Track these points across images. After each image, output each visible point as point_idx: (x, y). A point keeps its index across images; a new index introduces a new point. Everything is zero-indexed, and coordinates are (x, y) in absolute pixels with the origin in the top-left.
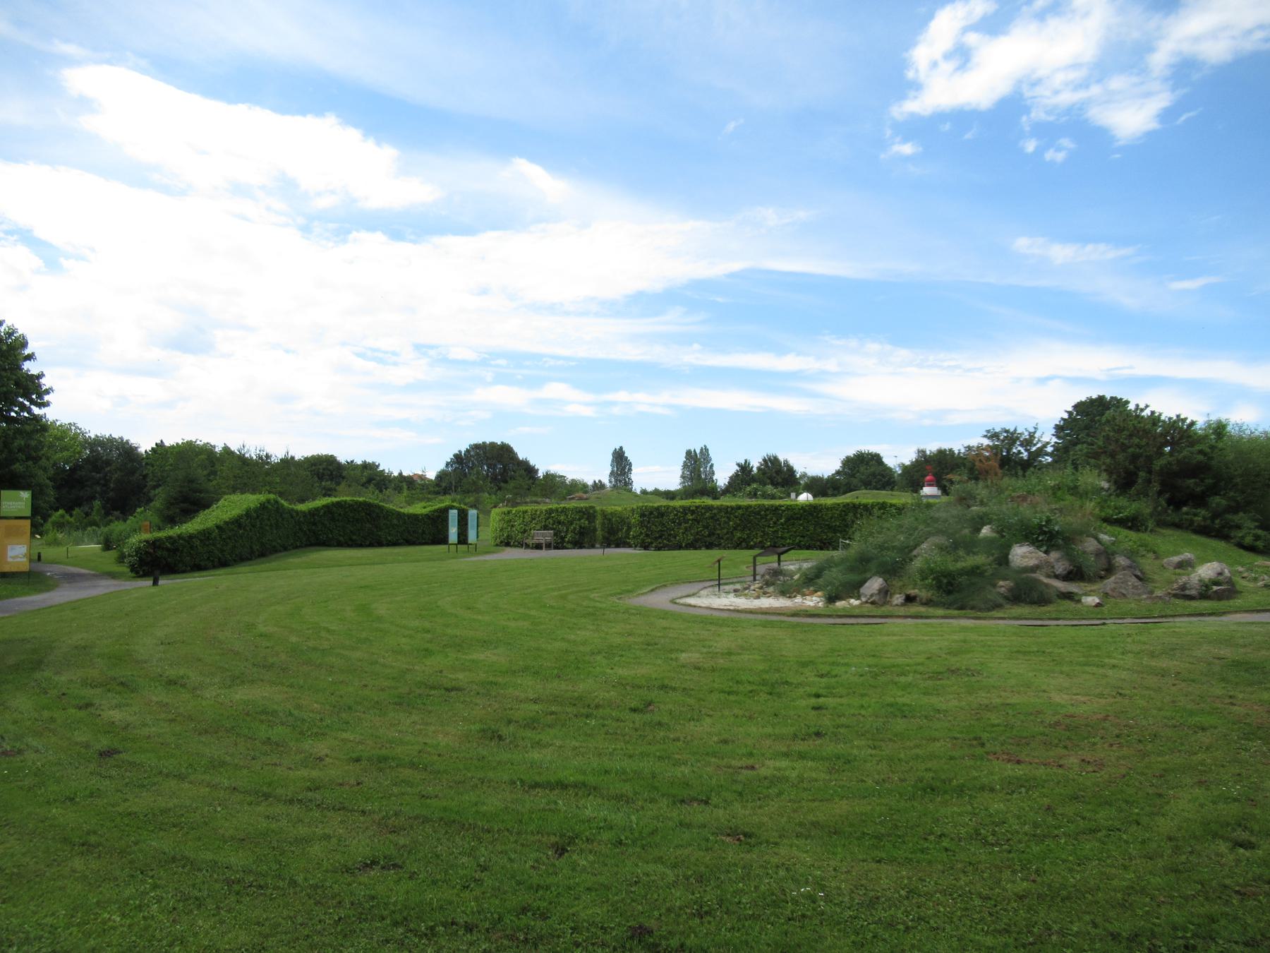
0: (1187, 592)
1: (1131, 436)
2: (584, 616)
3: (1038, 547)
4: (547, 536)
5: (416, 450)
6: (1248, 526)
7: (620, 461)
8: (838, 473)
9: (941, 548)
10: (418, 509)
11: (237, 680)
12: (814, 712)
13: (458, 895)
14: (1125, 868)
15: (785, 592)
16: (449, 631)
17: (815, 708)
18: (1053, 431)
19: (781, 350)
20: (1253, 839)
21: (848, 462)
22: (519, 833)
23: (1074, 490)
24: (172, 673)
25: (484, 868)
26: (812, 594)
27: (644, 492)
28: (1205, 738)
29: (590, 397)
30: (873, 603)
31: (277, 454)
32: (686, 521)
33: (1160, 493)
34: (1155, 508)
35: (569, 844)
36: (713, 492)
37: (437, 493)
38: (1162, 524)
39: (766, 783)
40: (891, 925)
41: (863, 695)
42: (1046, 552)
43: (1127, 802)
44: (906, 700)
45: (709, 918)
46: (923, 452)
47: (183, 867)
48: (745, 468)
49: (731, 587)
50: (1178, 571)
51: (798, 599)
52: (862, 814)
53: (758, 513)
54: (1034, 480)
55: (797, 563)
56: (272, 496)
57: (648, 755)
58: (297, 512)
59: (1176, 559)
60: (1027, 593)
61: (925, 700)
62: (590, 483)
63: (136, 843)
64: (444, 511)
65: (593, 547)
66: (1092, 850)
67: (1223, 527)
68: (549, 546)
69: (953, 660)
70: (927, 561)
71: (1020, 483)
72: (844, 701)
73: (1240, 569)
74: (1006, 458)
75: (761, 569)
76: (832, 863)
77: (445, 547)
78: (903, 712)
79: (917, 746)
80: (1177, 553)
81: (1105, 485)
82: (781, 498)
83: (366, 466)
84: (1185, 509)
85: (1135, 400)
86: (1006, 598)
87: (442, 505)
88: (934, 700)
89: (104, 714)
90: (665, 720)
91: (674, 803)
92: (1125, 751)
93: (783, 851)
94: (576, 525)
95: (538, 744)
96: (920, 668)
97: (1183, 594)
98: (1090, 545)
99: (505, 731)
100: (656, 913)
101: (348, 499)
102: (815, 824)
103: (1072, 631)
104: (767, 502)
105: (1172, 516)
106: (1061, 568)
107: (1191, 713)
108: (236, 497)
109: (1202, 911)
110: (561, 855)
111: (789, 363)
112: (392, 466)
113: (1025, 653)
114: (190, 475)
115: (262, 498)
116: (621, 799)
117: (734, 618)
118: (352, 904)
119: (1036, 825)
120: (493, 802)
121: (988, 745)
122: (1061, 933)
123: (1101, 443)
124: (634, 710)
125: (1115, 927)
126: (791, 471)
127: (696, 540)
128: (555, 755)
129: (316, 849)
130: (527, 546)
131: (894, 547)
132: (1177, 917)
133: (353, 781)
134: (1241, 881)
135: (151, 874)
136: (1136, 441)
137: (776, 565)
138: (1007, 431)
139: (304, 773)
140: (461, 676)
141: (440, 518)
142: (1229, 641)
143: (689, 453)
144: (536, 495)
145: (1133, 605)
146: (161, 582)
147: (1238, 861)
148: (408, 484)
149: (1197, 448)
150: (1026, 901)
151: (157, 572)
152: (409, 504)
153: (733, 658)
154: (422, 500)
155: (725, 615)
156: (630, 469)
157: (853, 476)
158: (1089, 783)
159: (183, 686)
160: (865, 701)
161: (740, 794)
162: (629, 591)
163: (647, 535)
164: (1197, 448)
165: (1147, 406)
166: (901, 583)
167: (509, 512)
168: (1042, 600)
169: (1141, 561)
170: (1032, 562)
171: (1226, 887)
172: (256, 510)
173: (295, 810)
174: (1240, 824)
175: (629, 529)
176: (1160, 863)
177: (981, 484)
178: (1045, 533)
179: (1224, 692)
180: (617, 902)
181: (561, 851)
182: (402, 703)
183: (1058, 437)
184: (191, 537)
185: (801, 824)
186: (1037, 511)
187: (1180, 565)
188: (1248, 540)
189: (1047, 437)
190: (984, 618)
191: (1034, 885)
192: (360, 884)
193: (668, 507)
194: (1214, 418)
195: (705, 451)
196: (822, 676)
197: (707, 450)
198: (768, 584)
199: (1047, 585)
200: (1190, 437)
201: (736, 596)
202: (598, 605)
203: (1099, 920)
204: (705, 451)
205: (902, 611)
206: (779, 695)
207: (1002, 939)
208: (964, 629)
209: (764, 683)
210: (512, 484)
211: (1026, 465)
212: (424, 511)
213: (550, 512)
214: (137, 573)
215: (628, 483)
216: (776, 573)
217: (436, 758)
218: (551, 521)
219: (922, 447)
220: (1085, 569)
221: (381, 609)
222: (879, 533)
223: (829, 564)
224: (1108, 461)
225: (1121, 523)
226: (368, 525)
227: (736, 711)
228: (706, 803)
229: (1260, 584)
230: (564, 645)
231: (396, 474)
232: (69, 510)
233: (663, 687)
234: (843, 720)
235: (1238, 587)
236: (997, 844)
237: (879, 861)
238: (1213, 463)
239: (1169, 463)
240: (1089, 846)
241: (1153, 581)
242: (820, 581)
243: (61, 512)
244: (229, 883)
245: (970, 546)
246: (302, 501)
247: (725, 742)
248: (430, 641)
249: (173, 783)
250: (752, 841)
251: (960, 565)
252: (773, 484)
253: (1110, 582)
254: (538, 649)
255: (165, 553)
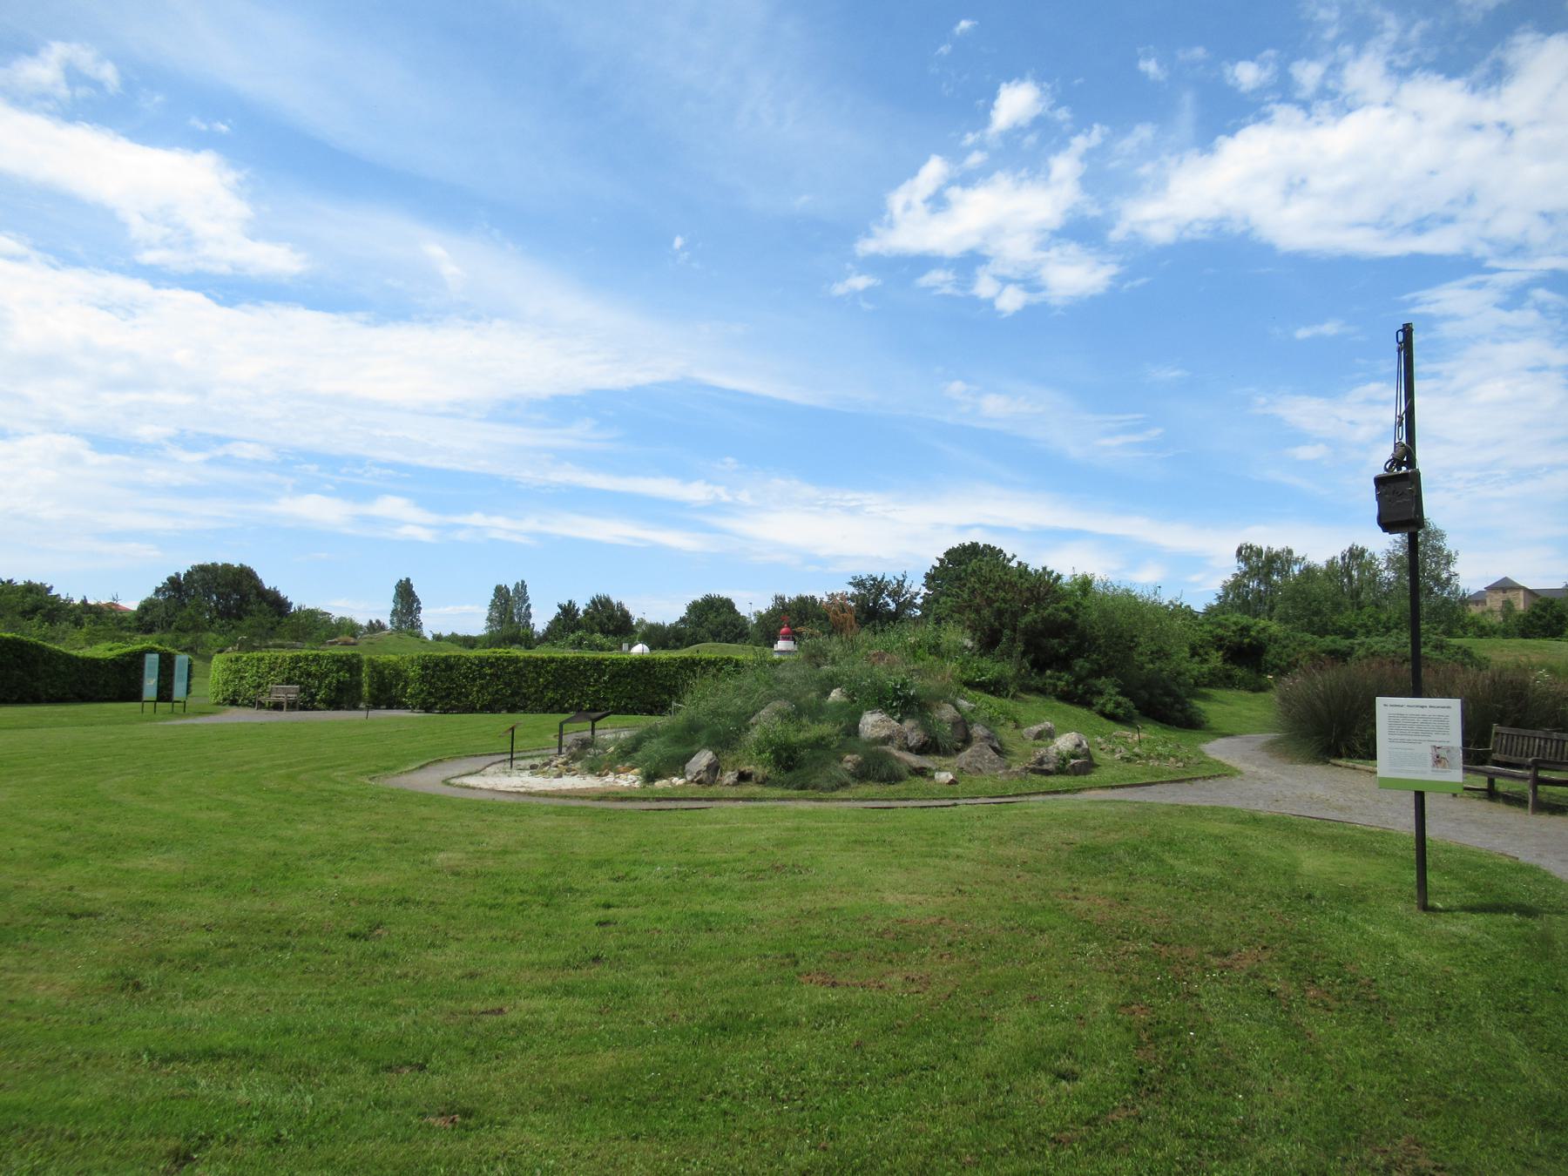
0: (1045, 767)
1: (997, 589)
2: (314, 803)
3: (892, 715)
7: (405, 594)
8: (682, 620)
9: (784, 716)
10: (102, 651)
12: (597, 930)
14: (933, 1118)
15: (594, 769)
16: (103, 827)
17: (601, 924)
19: (686, 475)
20: (1077, 1068)
21: (695, 608)
22: (121, 1138)
23: (935, 649)
27: (438, 638)
28: (1042, 942)
29: (432, 518)
30: (699, 782)
32: (482, 677)
33: (1024, 654)
35: (196, 1150)
36: (528, 640)
38: (1027, 689)
42: (900, 721)
48: (568, 611)
49: (530, 762)
50: (1039, 742)
51: (610, 778)
54: (893, 636)
55: (614, 731)
57: (356, 1002)
59: (1036, 729)
60: (876, 769)
61: (739, 907)
62: (365, 623)
64: (139, 656)
65: (355, 708)
68: (292, 706)
69: (779, 853)
72: (640, 911)
74: (872, 607)
75: (568, 739)
76: (574, 1146)
77: (139, 704)
78: (706, 924)
79: (719, 969)
80: (1038, 722)
81: (970, 644)
82: (610, 649)
83: (30, 588)
84: (1048, 672)
87: (139, 647)
88: (750, 905)
91: (376, 1072)
92: (955, 963)
93: (509, 1134)
94: (332, 679)
95: (195, 994)
96: (739, 866)
97: (1040, 769)
98: (947, 712)
99: (150, 975)
102: (564, 1089)
103: (919, 814)
104: (589, 655)
105: (1036, 681)
106: (915, 738)
107: (1031, 912)
111: (696, 492)
112: (71, 588)
113: (862, 843)
116: (304, 1071)
119: (840, 1069)
124: (353, 936)
126: (626, 616)
127: (495, 701)
128: (210, 1011)
130: (261, 706)
131: (728, 714)
137: (588, 734)
138: (874, 579)
140: (101, 894)
143: (499, 589)
144: (282, 637)
149: (1063, 604)
152: (91, 642)
153: (509, 858)
154: (113, 639)
157: (700, 625)
161: (473, 1052)
163: (430, 694)
164: (1063, 604)
166: (733, 759)
167: (237, 659)
168: (893, 778)
170: (884, 733)
174: (1067, 1048)
175: (406, 685)
177: (835, 639)
178: (899, 698)
185: (546, 1091)
187: (1039, 736)
188: (1109, 707)
189: (917, 587)
190: (827, 800)
191: (823, 1155)
194: (1080, 573)
195: (521, 589)
196: (617, 880)
197: (524, 586)
198: (574, 758)
199: (898, 759)
201: (533, 774)
202: (339, 787)
204: (521, 589)
205: (733, 792)
206: (558, 908)
208: (801, 814)
209: (541, 890)
210: (248, 621)
211: (895, 617)
212: (109, 655)
213: (297, 660)
215: (415, 626)
216: (585, 744)
217: (21, 1023)
218: (298, 673)
219: (780, 594)
222: (714, 695)
223: (652, 733)
225: (982, 687)
227: (497, 932)
228: (422, 1068)
230: (272, 845)
231: (77, 601)
234: (633, 938)
235: (1096, 761)
236: (789, 1099)
237: (636, 1138)
242: (638, 755)
245: (816, 712)
247: (472, 976)
250: (472, 1122)
251: (802, 736)
252: (602, 632)
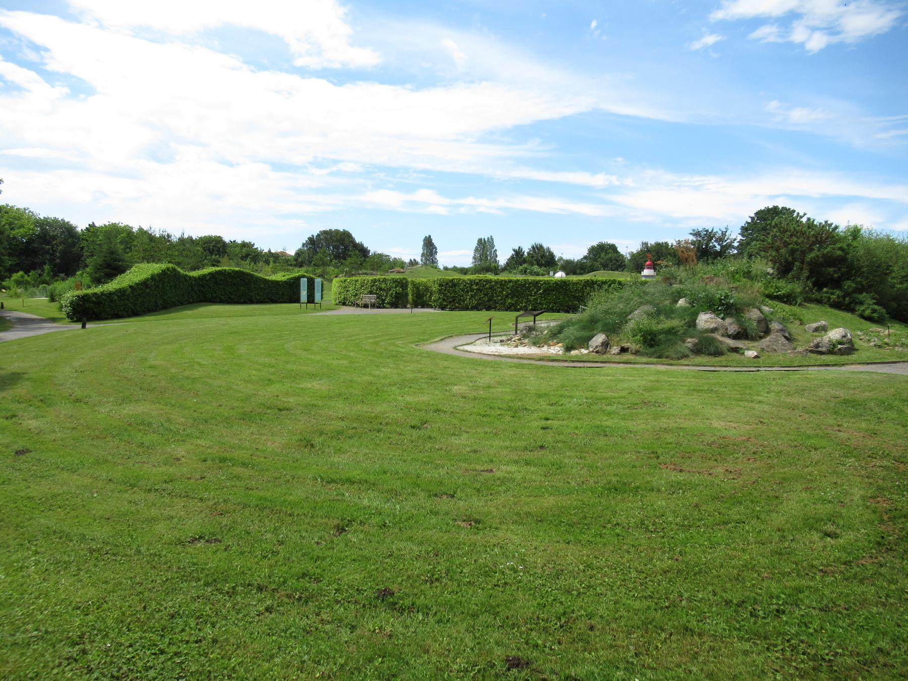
0: (820, 349)
1: (791, 236)
3: (718, 315)
4: (372, 299)
5: (280, 233)
6: (868, 304)
7: (429, 246)
8: (585, 257)
9: (649, 315)
10: (280, 277)
11: (126, 400)
12: (541, 431)
13: (257, 563)
14: (744, 550)
16: (289, 367)
18: (740, 231)
19: (593, 169)
20: (838, 531)
22: (312, 517)
23: (748, 274)
24: (79, 393)
25: (281, 543)
26: (554, 345)
27: (446, 269)
28: (815, 456)
29: (447, 201)
30: (597, 352)
31: (176, 235)
32: (472, 290)
33: (808, 278)
34: (804, 288)
35: (347, 526)
36: (496, 270)
37: (296, 266)
39: (498, 482)
40: (568, 592)
41: (579, 419)
42: (723, 319)
43: (752, 502)
44: (609, 423)
45: (438, 584)
46: (646, 244)
47: (60, 538)
48: (518, 253)
49: (499, 338)
51: (545, 349)
52: (562, 507)
53: (524, 286)
54: (720, 267)
55: (547, 322)
56: (171, 265)
58: (190, 277)
59: (815, 325)
60: (707, 347)
62: (407, 261)
63: (29, 520)
64: (297, 280)
65: (405, 307)
66: (722, 537)
67: (851, 303)
68: (373, 306)
69: (646, 395)
70: (638, 323)
71: (710, 267)
72: (565, 423)
73: (859, 333)
74: (705, 249)
75: (521, 326)
76: (535, 544)
78: (604, 432)
80: (815, 321)
81: (771, 271)
82: (543, 275)
83: (244, 245)
85: (799, 208)
86: (692, 350)
89: (25, 423)
90: (434, 434)
91: (430, 496)
93: (500, 534)
94: (393, 291)
95: (339, 451)
97: (816, 350)
99: (317, 440)
100: (399, 579)
101: (227, 268)
102: (528, 514)
103: (734, 375)
104: (531, 278)
105: (816, 295)
107: (809, 437)
108: (144, 265)
109: (793, 584)
110: (340, 533)
111: (599, 180)
112: (263, 245)
113: (698, 391)
114: (113, 248)
115: (163, 266)
116: (394, 493)
117: (496, 362)
118: (179, 568)
119: (685, 518)
120: (298, 493)
121: (661, 458)
122: (689, 600)
123: (769, 241)
124: (413, 427)
125: (727, 596)
126: (552, 256)
127: (478, 304)
128: (348, 459)
129: (160, 527)
130: (358, 306)
132: (774, 588)
133: (198, 476)
134: (825, 562)
135: (35, 543)
136: (795, 239)
138: (707, 231)
139: (164, 469)
141: (294, 284)
142: (842, 385)
143: (480, 241)
144: (366, 269)
145: (781, 357)
146: (87, 326)
147: (825, 547)
148: (275, 259)
149: (838, 245)
150: (669, 575)
151: (85, 319)
152: (274, 272)
153: (491, 390)
154: (284, 270)
155: (490, 359)
156: (436, 252)
157: (595, 260)
158: (728, 488)
159: (86, 403)
160: (579, 424)
161: (478, 490)
162: (424, 340)
163: (444, 300)
165: (805, 214)
166: (618, 339)
168: (718, 353)
169: (789, 325)
170: (713, 326)
171: (812, 566)
172: (159, 275)
173: (152, 497)
175: (431, 294)
176: (769, 548)
177: (682, 268)
178: (723, 305)
179: (835, 422)
180: (373, 570)
181: (341, 530)
182: (246, 417)
183: (743, 236)
184: (111, 294)
185: (518, 514)
186: (719, 288)
187: (816, 330)
188: (868, 312)
189: (735, 236)
192: (187, 553)
193: (459, 280)
194: (852, 224)
196: (552, 405)
197: (492, 239)
198: (524, 337)
199: (721, 342)
200: (833, 237)
202: (400, 349)
203: (718, 590)
207: (646, 603)
208: (659, 372)
209: (510, 409)
210: (349, 260)
211: (720, 254)
212: (284, 279)
213: (374, 281)
214: (72, 318)
215: (434, 262)
216: (531, 329)
217: (262, 459)
218: (376, 289)
220: (749, 331)
221: (243, 349)
222: (606, 302)
223: (569, 323)
224: (774, 253)
226: (242, 288)
227: (487, 429)
228: (453, 496)
229: (872, 344)
232: (27, 272)
233: (437, 411)
234: (562, 437)
235: (856, 346)
237: (568, 543)
238: (849, 256)
239: (818, 257)
240: (721, 534)
241: (797, 340)
242: (561, 336)
243: (21, 273)
244: (91, 551)
245: (669, 313)
246: (194, 269)
247: (475, 451)
248: (273, 374)
249: (65, 475)
250: (480, 526)
251: (660, 327)
252: (538, 265)
253: (766, 341)
254: (351, 381)
255: (92, 305)
